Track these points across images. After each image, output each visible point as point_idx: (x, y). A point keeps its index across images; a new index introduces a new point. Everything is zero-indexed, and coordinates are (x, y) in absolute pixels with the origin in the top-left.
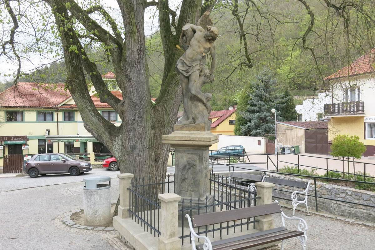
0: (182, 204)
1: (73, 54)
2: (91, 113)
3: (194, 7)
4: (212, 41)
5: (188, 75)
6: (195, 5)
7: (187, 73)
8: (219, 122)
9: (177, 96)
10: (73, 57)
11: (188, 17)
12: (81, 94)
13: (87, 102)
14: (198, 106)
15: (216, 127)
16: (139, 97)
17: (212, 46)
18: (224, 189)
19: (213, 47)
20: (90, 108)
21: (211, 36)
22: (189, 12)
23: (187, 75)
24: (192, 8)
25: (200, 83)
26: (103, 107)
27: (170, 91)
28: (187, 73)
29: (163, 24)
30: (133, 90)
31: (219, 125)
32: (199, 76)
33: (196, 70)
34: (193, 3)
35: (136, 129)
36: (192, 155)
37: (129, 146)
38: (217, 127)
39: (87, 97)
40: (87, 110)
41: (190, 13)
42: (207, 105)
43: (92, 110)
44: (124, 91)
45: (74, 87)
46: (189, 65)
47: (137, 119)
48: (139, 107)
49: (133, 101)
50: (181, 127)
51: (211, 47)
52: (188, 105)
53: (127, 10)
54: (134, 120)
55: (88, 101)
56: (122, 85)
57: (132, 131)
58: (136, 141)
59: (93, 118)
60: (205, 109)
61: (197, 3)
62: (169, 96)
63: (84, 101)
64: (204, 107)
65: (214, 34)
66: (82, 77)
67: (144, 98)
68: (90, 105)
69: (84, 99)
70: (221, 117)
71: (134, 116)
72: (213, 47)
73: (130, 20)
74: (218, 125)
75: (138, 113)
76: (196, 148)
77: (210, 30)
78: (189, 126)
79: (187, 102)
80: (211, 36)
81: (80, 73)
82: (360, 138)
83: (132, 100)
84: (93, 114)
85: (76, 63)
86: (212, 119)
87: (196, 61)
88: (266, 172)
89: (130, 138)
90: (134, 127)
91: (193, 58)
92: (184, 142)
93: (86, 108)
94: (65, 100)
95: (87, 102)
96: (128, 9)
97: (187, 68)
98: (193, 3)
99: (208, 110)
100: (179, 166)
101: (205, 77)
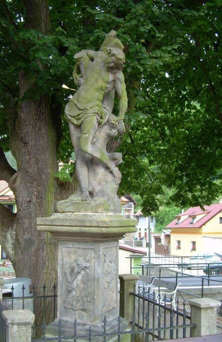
0: (58, 328)
5: (79, 122)
7: (78, 119)
8: (206, 220)
15: (201, 227)
16: (39, 169)
18: (175, 306)
21: (113, 62)
23: (77, 124)
28: (78, 119)
30: (30, 159)
31: (206, 224)
32: (99, 125)
33: (92, 114)
35: (33, 215)
36: (84, 251)
37: (24, 240)
38: (204, 226)
44: (19, 161)
46: (82, 108)
47: (34, 200)
48: (38, 184)
49: (29, 174)
54: (30, 201)
56: (16, 151)
57: (27, 217)
58: (32, 234)
65: (117, 58)
67: (45, 170)
70: (209, 213)
71: (29, 196)
74: (204, 224)
75: (36, 192)
76: (89, 239)
77: (110, 53)
80: (113, 62)
83: (29, 172)
86: (196, 216)
88: (178, 274)
89: (25, 228)
90: (30, 212)
92: (70, 228)
94: (4, 190)
97: (78, 112)
99: (116, 179)
100: (64, 268)
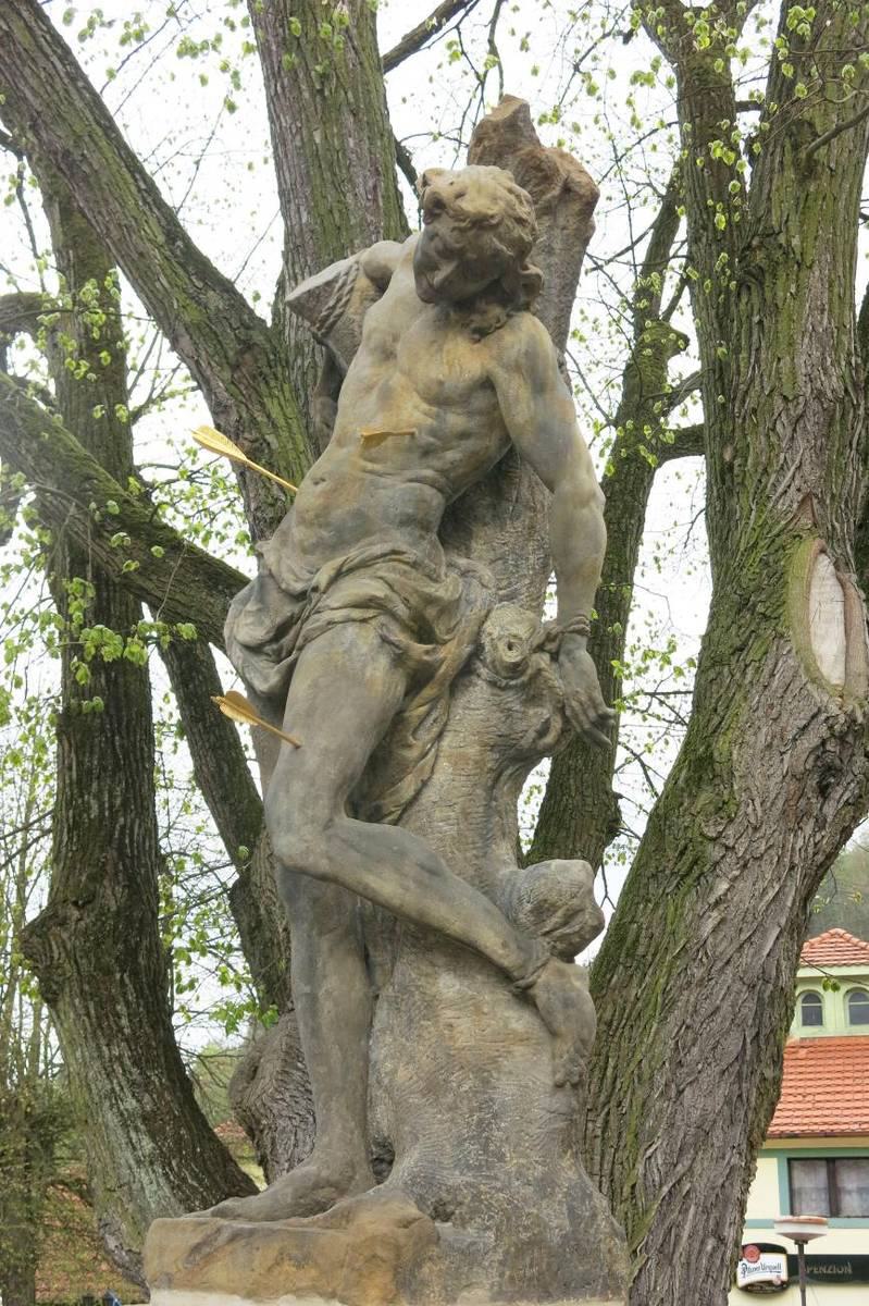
1: (92, 753)
2: (133, 1135)
3: (775, 276)
4: (496, 311)
6: (778, 255)
9: (699, 973)
10: (90, 772)
11: (744, 355)
12: (91, 1006)
13: (120, 1058)
14: (430, 1006)
17: (499, 359)
19: (516, 368)
20: (130, 1104)
22: (749, 317)
24: (761, 284)
25: (458, 760)
26: (794, 1136)
27: (643, 941)
29: (719, 497)
34: (761, 246)
39: (124, 1022)
40: (111, 1118)
41: (756, 319)
42: (540, 994)
43: (145, 1119)
45: (56, 956)
50: (196, 1248)
51: (501, 375)
52: (313, 998)
53: (227, 375)
55: (127, 1054)
59: (143, 1176)
60: (523, 1040)
61: (795, 242)
62: (635, 980)
63: (101, 1056)
64: (519, 1020)
66: (119, 889)
68: (133, 1083)
69: (103, 1041)
72: (517, 368)
73: (255, 435)
78: (252, 1232)
79: (311, 962)
81: (109, 868)
82: (237, 104)
84: (147, 1145)
85: (101, 806)
87: (368, 533)
91: (337, 514)
93: (107, 1104)
95: (120, 1058)
96: (235, 367)
98: (761, 246)
99: (558, 1043)
101: (493, 684)
